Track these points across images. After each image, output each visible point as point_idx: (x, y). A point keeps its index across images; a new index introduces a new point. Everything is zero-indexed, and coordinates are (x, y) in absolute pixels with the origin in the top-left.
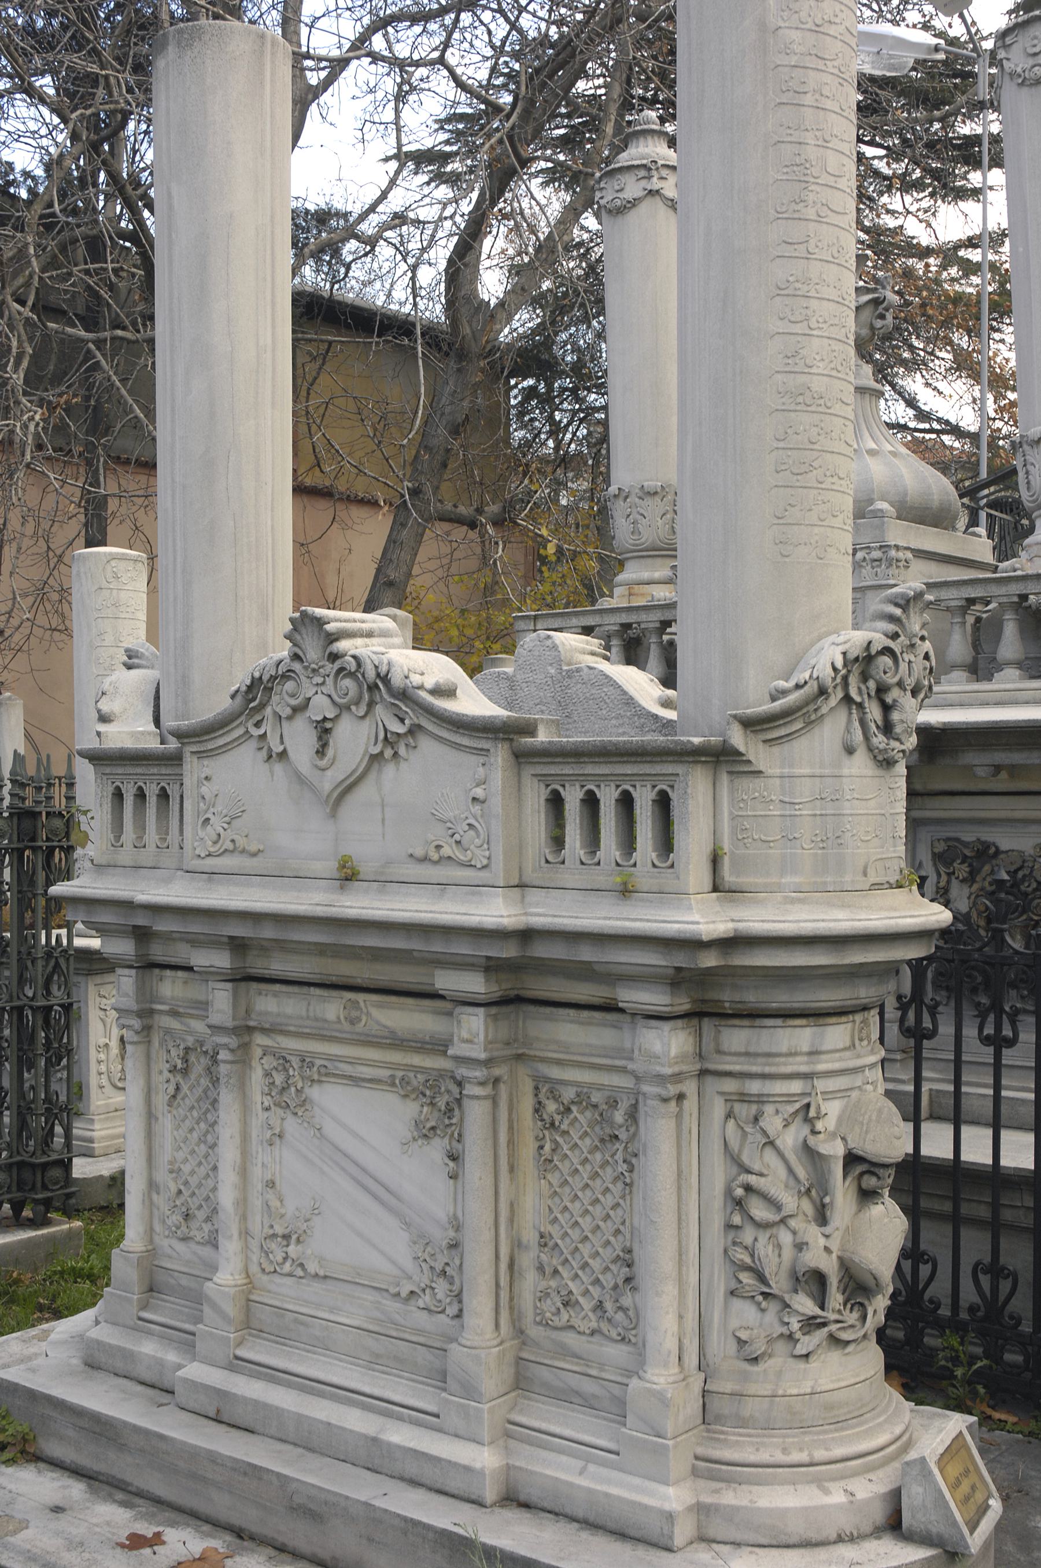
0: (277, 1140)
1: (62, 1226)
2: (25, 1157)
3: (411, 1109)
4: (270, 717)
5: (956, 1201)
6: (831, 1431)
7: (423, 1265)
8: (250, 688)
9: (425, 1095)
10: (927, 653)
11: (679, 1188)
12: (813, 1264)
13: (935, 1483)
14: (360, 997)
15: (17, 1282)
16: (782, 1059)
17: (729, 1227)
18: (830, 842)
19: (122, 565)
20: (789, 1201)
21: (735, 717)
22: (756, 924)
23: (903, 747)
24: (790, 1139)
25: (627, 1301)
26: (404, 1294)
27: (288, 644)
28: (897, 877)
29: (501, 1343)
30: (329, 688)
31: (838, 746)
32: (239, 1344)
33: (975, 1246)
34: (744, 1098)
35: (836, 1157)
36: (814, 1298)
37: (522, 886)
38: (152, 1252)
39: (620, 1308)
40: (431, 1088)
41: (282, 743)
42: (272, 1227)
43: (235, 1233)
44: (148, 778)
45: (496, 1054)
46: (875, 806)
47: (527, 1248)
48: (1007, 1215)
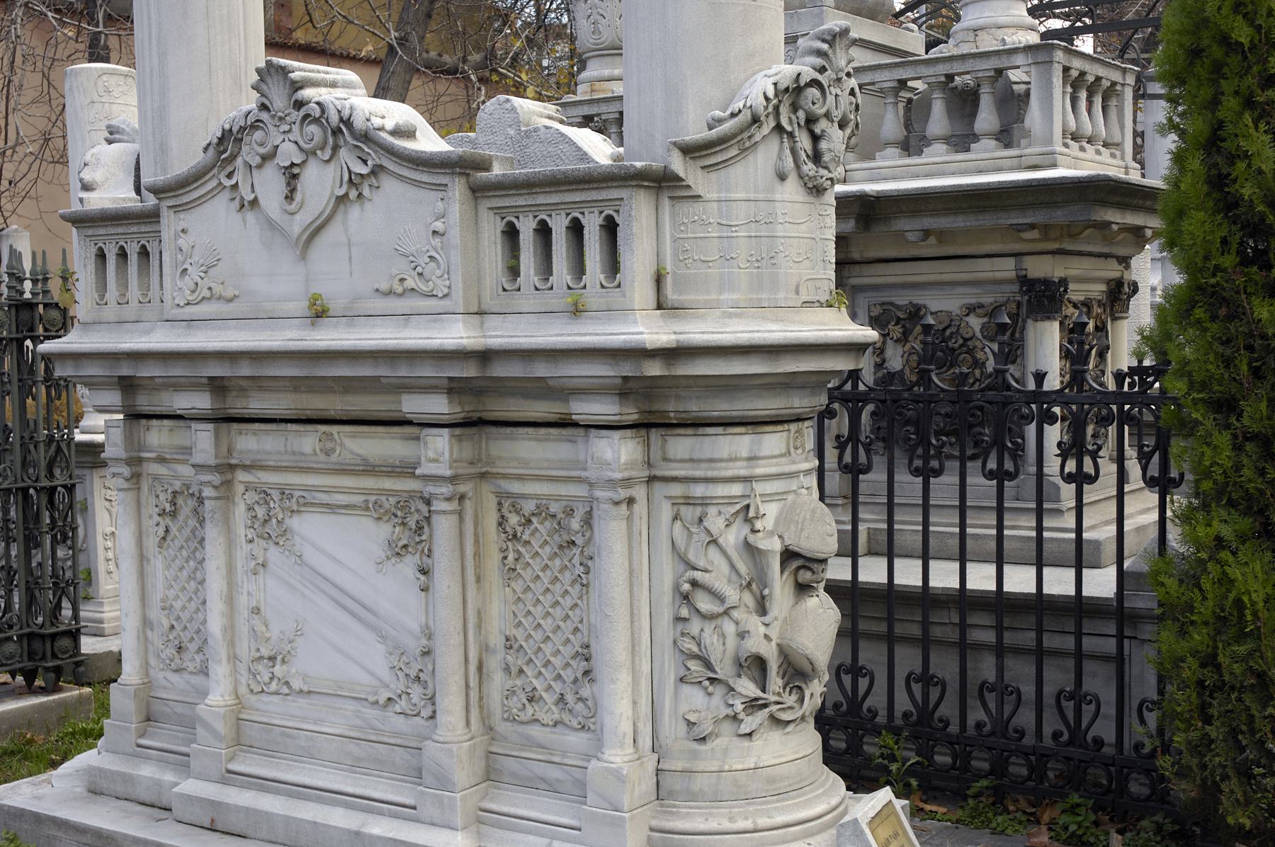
0: (261, 569)
2: (36, 630)
3: (385, 530)
4: (241, 167)
5: (890, 621)
6: (773, 802)
7: (399, 673)
8: (221, 140)
9: (396, 516)
10: (852, 89)
11: (631, 586)
12: (754, 650)
13: (867, 842)
14: (334, 429)
15: (30, 742)
16: (723, 464)
17: (679, 619)
18: (764, 262)
20: (732, 594)
21: (675, 144)
22: (697, 336)
23: (830, 175)
24: (732, 538)
25: (586, 692)
28: (827, 297)
29: (472, 739)
30: (295, 135)
32: (231, 760)
33: (908, 659)
34: (689, 501)
35: (773, 552)
36: (755, 682)
37: (481, 313)
38: (148, 684)
39: (580, 699)
40: (402, 508)
41: (253, 191)
42: (258, 650)
43: (224, 657)
44: (127, 236)
45: (461, 471)
46: (806, 236)
47: (494, 651)
48: (936, 632)
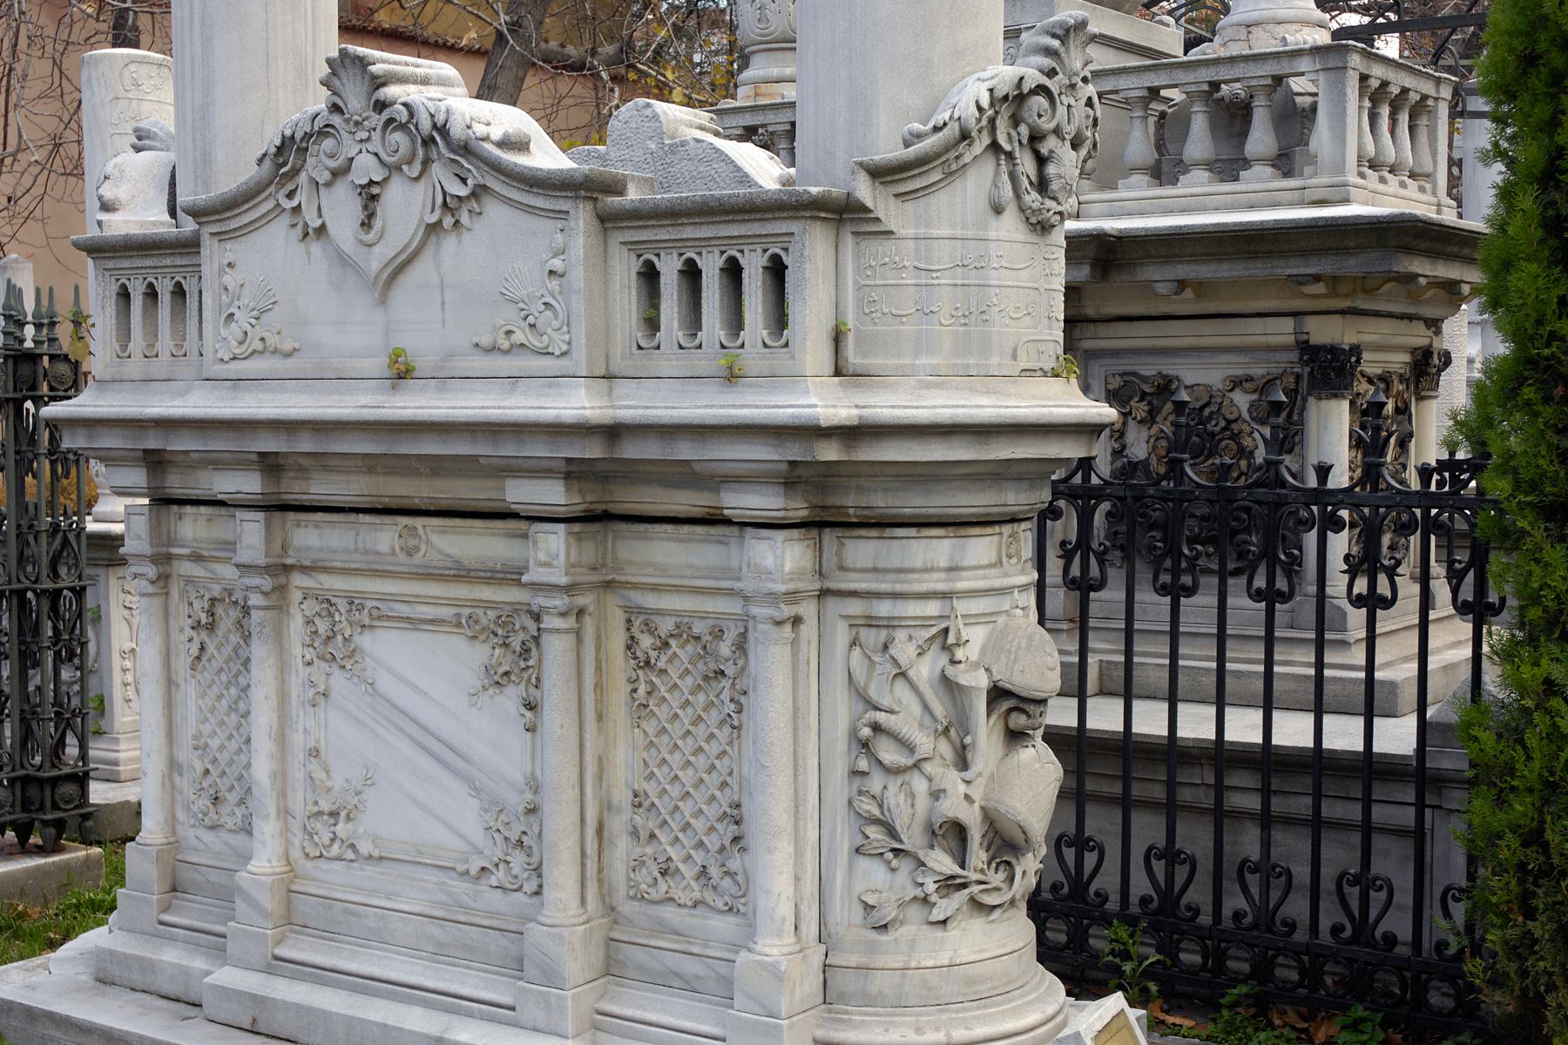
0: (322, 700)
1: (77, 854)
2: (31, 772)
3: (481, 653)
5: (1127, 781)
6: (972, 1009)
7: (496, 835)
8: (280, 150)
10: (1090, 99)
11: (795, 729)
12: (951, 814)
14: (419, 522)
15: (23, 916)
16: (917, 576)
17: (856, 773)
18: (973, 317)
19: (143, 71)
20: (924, 742)
21: (861, 164)
23: (1059, 208)
24: (925, 670)
25: (734, 864)
26: (474, 871)
27: (325, 93)
28: (1053, 364)
29: (588, 921)
30: (375, 145)
31: (983, 203)
32: (278, 943)
33: (1148, 830)
34: (871, 622)
37: (609, 377)
38: (174, 844)
39: (727, 873)
41: (320, 216)
42: (316, 803)
43: (272, 810)
44: (160, 271)
45: (580, 579)
46: (1030, 285)
47: (619, 810)
48: (1185, 795)
